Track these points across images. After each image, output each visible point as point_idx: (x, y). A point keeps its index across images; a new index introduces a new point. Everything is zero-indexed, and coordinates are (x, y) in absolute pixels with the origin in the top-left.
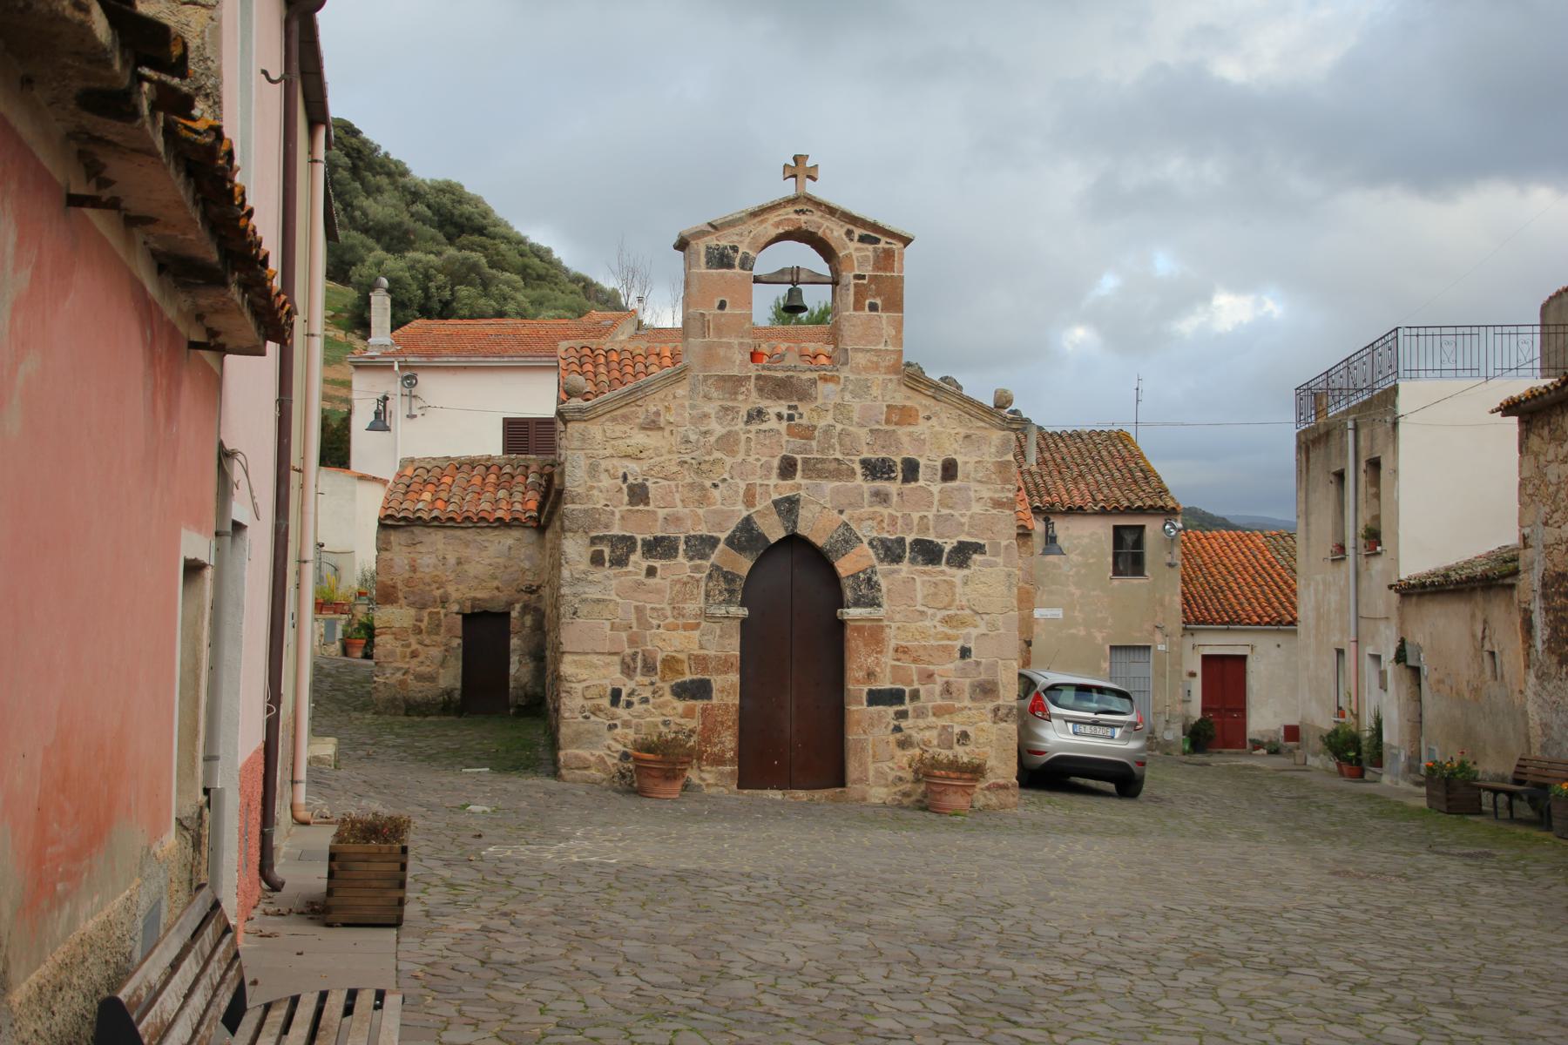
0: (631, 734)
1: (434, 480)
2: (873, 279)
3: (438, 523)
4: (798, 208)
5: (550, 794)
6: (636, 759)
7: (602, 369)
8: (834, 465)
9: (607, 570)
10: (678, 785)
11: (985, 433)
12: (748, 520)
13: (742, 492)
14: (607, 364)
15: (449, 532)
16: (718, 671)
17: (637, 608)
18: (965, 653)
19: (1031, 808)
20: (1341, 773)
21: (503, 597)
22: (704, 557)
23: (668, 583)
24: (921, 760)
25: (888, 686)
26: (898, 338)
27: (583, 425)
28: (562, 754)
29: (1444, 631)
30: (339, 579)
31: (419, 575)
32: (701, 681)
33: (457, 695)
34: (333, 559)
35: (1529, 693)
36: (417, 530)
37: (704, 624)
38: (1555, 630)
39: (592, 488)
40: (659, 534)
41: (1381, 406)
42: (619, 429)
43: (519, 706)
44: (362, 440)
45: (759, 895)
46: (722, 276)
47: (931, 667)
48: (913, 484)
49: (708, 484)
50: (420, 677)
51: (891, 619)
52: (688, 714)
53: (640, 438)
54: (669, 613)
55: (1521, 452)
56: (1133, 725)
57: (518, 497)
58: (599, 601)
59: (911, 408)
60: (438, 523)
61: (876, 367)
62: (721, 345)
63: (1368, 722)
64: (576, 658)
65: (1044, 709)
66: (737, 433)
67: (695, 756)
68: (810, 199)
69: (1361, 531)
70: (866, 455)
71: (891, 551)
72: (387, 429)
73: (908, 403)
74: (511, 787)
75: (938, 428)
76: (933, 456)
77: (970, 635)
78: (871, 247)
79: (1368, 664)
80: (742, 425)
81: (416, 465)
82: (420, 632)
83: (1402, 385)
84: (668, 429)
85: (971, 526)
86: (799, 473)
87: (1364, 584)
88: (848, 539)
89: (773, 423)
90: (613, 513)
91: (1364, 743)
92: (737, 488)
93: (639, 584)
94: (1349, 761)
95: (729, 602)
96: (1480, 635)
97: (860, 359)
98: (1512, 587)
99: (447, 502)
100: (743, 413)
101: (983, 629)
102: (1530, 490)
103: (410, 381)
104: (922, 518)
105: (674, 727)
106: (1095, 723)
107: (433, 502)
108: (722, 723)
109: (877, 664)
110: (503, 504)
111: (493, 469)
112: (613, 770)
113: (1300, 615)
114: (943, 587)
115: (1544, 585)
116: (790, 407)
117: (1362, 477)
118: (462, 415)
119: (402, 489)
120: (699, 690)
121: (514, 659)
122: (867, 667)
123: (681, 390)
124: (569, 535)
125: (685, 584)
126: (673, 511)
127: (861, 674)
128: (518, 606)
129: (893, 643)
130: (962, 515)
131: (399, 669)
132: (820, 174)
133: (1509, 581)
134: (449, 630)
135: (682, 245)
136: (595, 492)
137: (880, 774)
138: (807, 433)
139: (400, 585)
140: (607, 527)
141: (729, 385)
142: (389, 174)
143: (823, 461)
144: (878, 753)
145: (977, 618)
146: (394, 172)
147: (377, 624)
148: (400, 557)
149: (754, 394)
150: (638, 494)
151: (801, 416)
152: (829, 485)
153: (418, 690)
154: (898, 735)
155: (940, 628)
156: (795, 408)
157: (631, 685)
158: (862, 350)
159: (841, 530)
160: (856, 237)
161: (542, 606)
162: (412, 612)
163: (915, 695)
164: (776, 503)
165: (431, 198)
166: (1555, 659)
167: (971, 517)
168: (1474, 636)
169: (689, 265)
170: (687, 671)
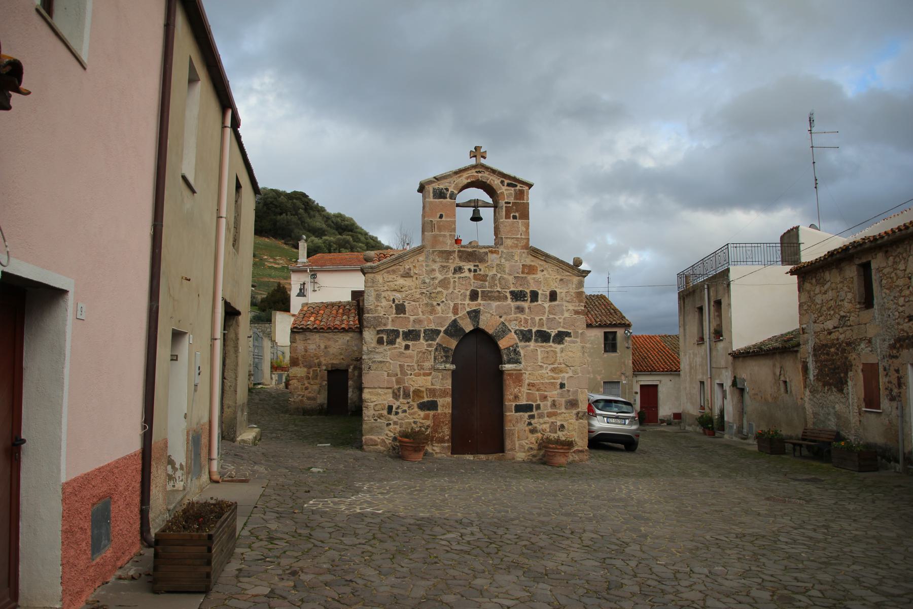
0: (398, 428)
5: (356, 459)
6: (400, 441)
8: (497, 294)
9: (385, 347)
10: (422, 453)
12: (455, 321)
16: (441, 397)
18: (562, 386)
19: (593, 460)
20: (705, 434)
21: (345, 363)
22: (434, 340)
23: (415, 353)
24: (542, 439)
25: (525, 403)
29: (759, 374)
33: (325, 406)
34: (282, 349)
35: (806, 399)
36: (307, 334)
38: (821, 370)
41: (722, 279)
42: (391, 277)
45: (469, 543)
49: (435, 303)
50: (309, 398)
51: (526, 370)
53: (401, 281)
54: (416, 367)
55: (799, 290)
56: (633, 418)
57: (352, 319)
58: (381, 362)
62: (440, 236)
63: (716, 412)
65: (593, 411)
67: (429, 439)
68: (483, 166)
69: (712, 330)
70: (512, 289)
71: (525, 336)
72: (305, 296)
74: (338, 456)
75: (547, 276)
76: (545, 289)
77: (565, 377)
79: (716, 387)
83: (731, 268)
86: (480, 298)
87: (714, 353)
88: (504, 330)
89: (467, 274)
91: (715, 421)
92: (450, 306)
94: (709, 428)
95: (445, 362)
96: (778, 374)
97: (509, 242)
98: (797, 351)
100: (452, 268)
101: (570, 374)
102: (805, 307)
103: (314, 276)
105: (419, 425)
106: (617, 418)
110: (345, 322)
113: (682, 366)
114: (551, 354)
115: (815, 350)
117: (712, 308)
118: (337, 287)
120: (431, 406)
121: (350, 390)
122: (516, 394)
126: (419, 316)
127: (511, 397)
128: (352, 367)
129: (527, 382)
130: (559, 318)
132: (488, 156)
135: (421, 189)
136: (379, 308)
137: (522, 446)
138: (483, 278)
141: (445, 255)
142: (318, 211)
143: (491, 292)
144: (521, 438)
146: (320, 210)
149: (457, 259)
150: (400, 309)
152: (495, 304)
153: (308, 404)
155: (550, 374)
157: (398, 403)
163: (538, 407)
164: (468, 313)
166: (821, 384)
168: (775, 374)
169: (424, 197)
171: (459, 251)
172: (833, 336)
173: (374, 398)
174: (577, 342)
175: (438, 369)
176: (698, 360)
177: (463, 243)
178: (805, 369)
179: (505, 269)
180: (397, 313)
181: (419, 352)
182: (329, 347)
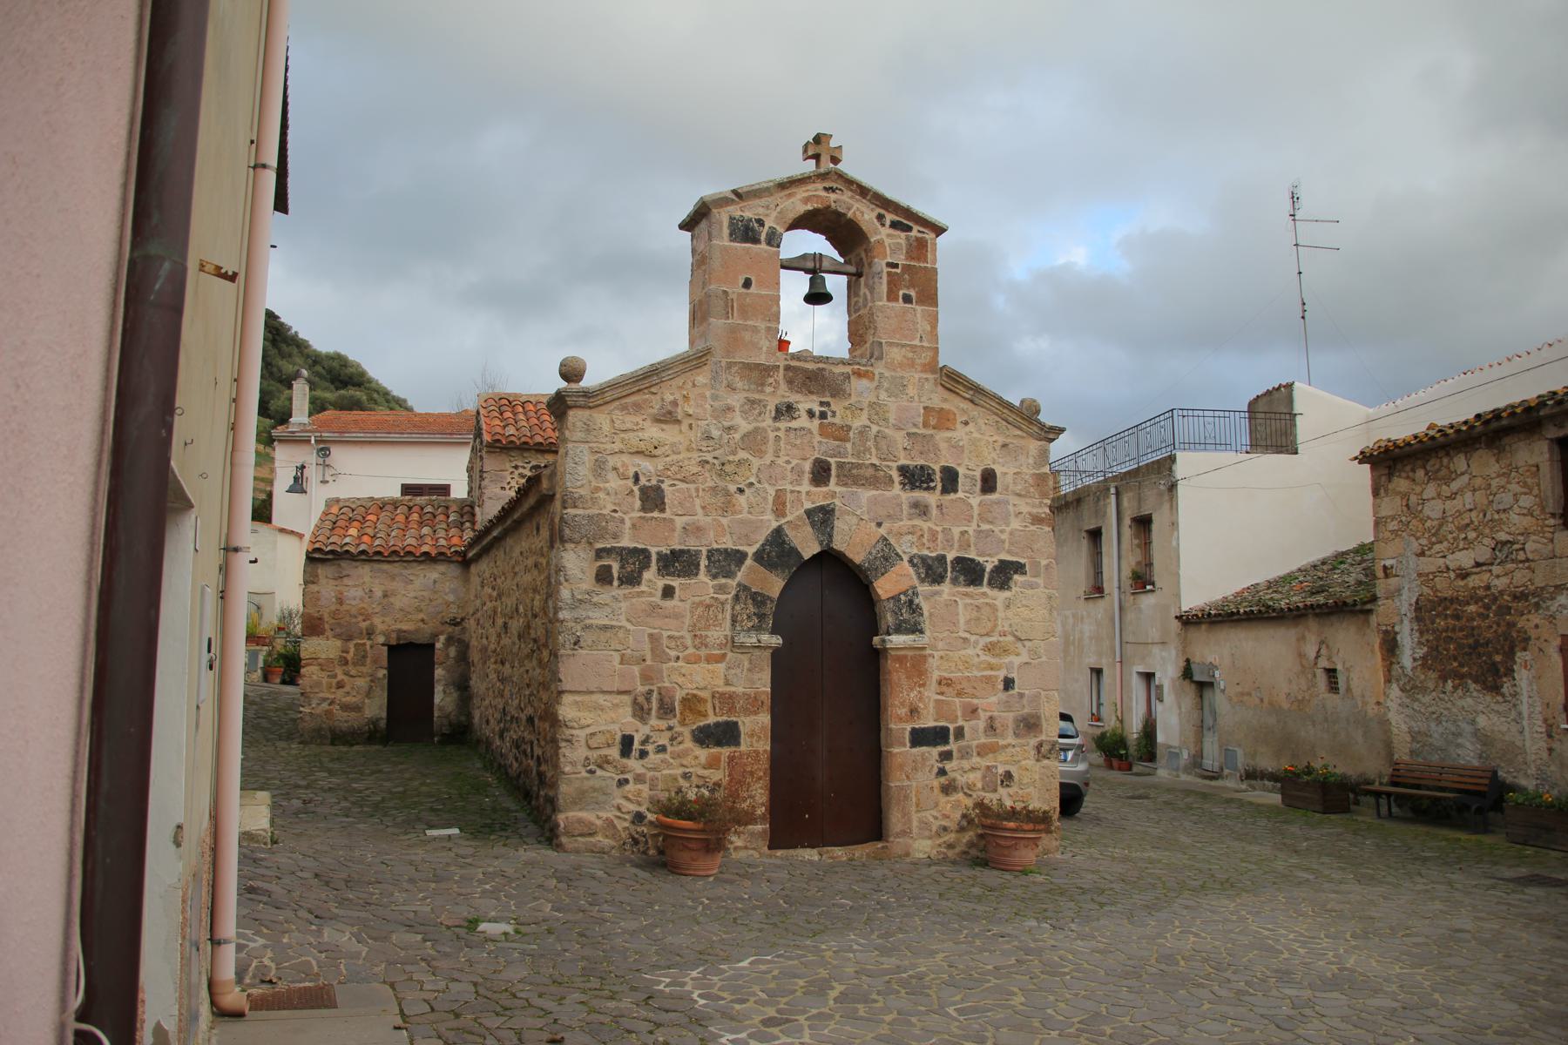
2: (907, 268)
3: (364, 557)
4: (827, 185)
7: (522, 417)
8: (870, 471)
9: (616, 590)
11: (1023, 442)
12: (778, 532)
13: (770, 499)
14: (525, 413)
15: (376, 566)
17: (651, 636)
18: (1008, 684)
20: (1111, 767)
21: (428, 629)
23: (688, 605)
25: (931, 724)
26: (934, 336)
27: (587, 413)
28: (561, 818)
29: (1267, 656)
30: (261, 616)
32: (727, 723)
33: (383, 724)
35: (1393, 705)
36: (344, 564)
37: (730, 655)
39: (598, 489)
40: (677, 547)
41: (1159, 473)
42: (630, 420)
44: (284, 504)
46: (747, 251)
47: (975, 701)
48: (952, 496)
49: (733, 488)
50: (346, 707)
52: (713, 763)
53: (653, 432)
54: (689, 642)
56: (1080, 747)
57: (442, 533)
58: (605, 628)
59: (949, 412)
60: (364, 557)
61: (912, 364)
62: (746, 328)
63: (1135, 727)
64: (578, 698)
66: (764, 430)
69: (1126, 573)
71: (932, 570)
73: (946, 406)
75: (976, 435)
77: (1013, 663)
78: (903, 235)
80: (769, 422)
82: (346, 663)
83: (1179, 455)
84: (686, 422)
85: (1011, 544)
86: (833, 480)
88: (888, 557)
89: (803, 421)
90: (622, 521)
92: (765, 501)
93: (655, 607)
95: (758, 629)
96: (1312, 655)
97: (895, 354)
98: (1370, 611)
99: (374, 537)
100: (771, 407)
101: (1024, 658)
103: (324, 452)
104: (963, 533)
105: (695, 780)
107: (359, 537)
108: (752, 773)
110: (428, 540)
114: (986, 611)
115: (1418, 608)
116: (822, 404)
117: (1127, 532)
119: (328, 525)
120: (725, 734)
121: (438, 689)
122: (909, 703)
123: (702, 378)
124: (569, 546)
125: (708, 607)
126: (694, 520)
127: (903, 711)
128: (442, 638)
129: (936, 675)
131: (324, 700)
133: (1368, 607)
134: (375, 661)
135: (695, 221)
136: (602, 495)
137: (925, 825)
138: (842, 433)
139: (326, 617)
140: (615, 537)
141: (755, 374)
143: (859, 466)
145: (1019, 645)
148: (327, 589)
149: (783, 386)
150: (652, 498)
151: (834, 413)
152: (866, 494)
153: (344, 720)
154: (942, 780)
156: (828, 404)
157: (645, 730)
159: (880, 546)
161: (466, 637)
162: (339, 643)
163: (960, 733)
164: (809, 513)
165: (326, 364)
166: (1433, 675)
167: (1011, 533)
168: (1301, 655)
171: (787, 368)
172: (1473, 581)
173: (587, 717)
174: (1038, 586)
175: (742, 646)
176: (1088, 629)
177: (792, 349)
178: (1390, 645)
179: (889, 411)
180: (643, 509)
181: (696, 605)
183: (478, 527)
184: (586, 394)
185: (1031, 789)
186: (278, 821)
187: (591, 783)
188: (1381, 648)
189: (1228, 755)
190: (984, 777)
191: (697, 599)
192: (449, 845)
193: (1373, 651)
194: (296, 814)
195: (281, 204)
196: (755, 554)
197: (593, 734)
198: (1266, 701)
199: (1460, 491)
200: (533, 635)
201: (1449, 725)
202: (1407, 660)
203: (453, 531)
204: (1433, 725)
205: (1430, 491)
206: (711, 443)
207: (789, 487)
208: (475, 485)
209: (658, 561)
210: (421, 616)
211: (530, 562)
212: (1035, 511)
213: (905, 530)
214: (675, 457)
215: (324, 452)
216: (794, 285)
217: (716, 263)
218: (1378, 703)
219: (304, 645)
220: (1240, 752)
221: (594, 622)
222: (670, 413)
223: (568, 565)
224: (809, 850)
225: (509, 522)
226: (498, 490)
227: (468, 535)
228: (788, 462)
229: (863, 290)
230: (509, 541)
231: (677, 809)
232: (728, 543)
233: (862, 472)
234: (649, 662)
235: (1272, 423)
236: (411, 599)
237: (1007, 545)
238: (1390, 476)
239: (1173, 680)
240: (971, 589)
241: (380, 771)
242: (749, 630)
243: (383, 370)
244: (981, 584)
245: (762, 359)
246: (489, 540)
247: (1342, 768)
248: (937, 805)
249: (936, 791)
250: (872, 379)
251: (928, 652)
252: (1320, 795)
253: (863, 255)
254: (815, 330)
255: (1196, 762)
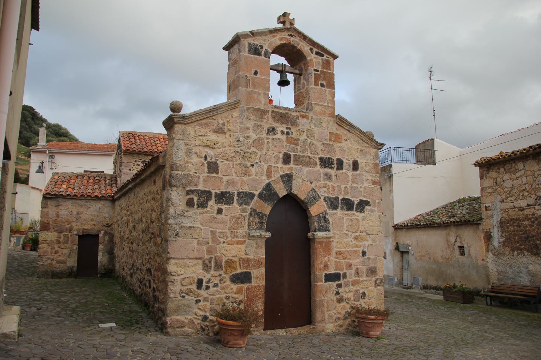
1: (67, 181)
2: (322, 72)
3: (69, 197)
4: (290, 33)
7: (138, 141)
9: (196, 210)
11: (368, 149)
12: (269, 185)
13: (265, 170)
14: (139, 140)
15: (74, 201)
16: (255, 267)
18: (364, 253)
21: (96, 228)
22: (247, 204)
23: (228, 218)
26: (333, 102)
27: (183, 126)
29: (434, 242)
30: (22, 223)
31: (60, 219)
32: (246, 273)
33: (75, 269)
34: (21, 216)
36: (60, 200)
37: (247, 241)
39: (188, 162)
40: (224, 191)
42: (203, 131)
43: (102, 274)
47: (351, 261)
48: (341, 171)
49: (249, 164)
50: (58, 262)
51: (334, 238)
53: (213, 137)
54: (229, 235)
57: (103, 188)
58: (191, 228)
59: (339, 135)
60: (69, 197)
61: (324, 114)
62: (255, 92)
64: (177, 261)
70: (321, 156)
71: (333, 204)
73: (338, 132)
75: (350, 145)
77: (366, 244)
78: (321, 58)
80: (265, 135)
81: (59, 175)
83: (394, 165)
85: (365, 193)
86: (292, 162)
88: (315, 197)
89: (279, 136)
90: (199, 177)
93: (213, 218)
95: (260, 229)
96: (453, 241)
97: (317, 109)
98: (479, 224)
99: (73, 189)
101: (370, 242)
103: (52, 157)
107: (67, 189)
108: (257, 296)
109: (329, 260)
110: (97, 190)
111: (91, 178)
112: (198, 326)
114: (355, 222)
115: (501, 222)
116: (287, 128)
119: (53, 183)
120: (245, 278)
121: (100, 254)
122: (324, 262)
125: (238, 218)
126: (230, 178)
127: (321, 266)
129: (335, 250)
131: (49, 258)
133: (479, 222)
134: (72, 242)
137: (331, 317)
138: (295, 142)
139: (51, 223)
140: (196, 185)
141: (259, 113)
143: (303, 157)
144: (331, 309)
145: (368, 236)
147: (40, 239)
148: (52, 211)
149: (271, 119)
150: (213, 168)
151: (292, 133)
152: (306, 169)
153: (58, 267)
154: (338, 296)
156: (290, 129)
157: (208, 276)
158: (319, 105)
159: (312, 192)
160: (314, 52)
162: (56, 234)
163: (345, 276)
164: (282, 177)
167: (364, 188)
168: (448, 241)
170: (238, 267)
171: (273, 112)
172: (526, 212)
173: (181, 271)
175: (253, 237)
177: (274, 104)
178: (488, 237)
182: (82, 213)
183: (119, 186)
184: (184, 117)
185: (373, 300)
186: (24, 321)
187: (183, 302)
188: (484, 238)
189: (415, 280)
190: (354, 295)
191: (233, 215)
192: (112, 333)
193: (480, 240)
194: (33, 316)
195: (35, 25)
196: (259, 194)
197: (184, 279)
198: (432, 259)
199: (521, 177)
200: (151, 231)
201: (516, 268)
202: (496, 242)
203: (108, 187)
204: (508, 269)
205: (507, 176)
206: (239, 143)
207: (273, 165)
208: (117, 169)
209: (215, 196)
210: (93, 223)
211: (150, 198)
212: (373, 179)
213: (322, 185)
214: (223, 149)
215: (52, 157)
216: (275, 77)
217: (242, 63)
218: (483, 260)
219: (40, 235)
220: (420, 278)
221: (186, 225)
222: (221, 128)
223: (174, 198)
224: (281, 330)
225: (138, 180)
226: (128, 171)
227: (115, 189)
228: (273, 154)
229: (302, 81)
230: (137, 189)
231: (225, 314)
232: (247, 189)
233: (304, 159)
234: (210, 244)
235: (425, 153)
236: (90, 216)
237: (363, 193)
238: (488, 171)
239: (390, 250)
240: (349, 212)
241: (74, 291)
242: (256, 229)
243: (73, 131)
244: (352, 210)
245: (262, 107)
246: (125, 190)
247: (470, 286)
248: (335, 307)
249: (335, 302)
250: (308, 119)
251: (332, 240)
252: (461, 297)
253: (303, 66)
254: (285, 98)
255: (400, 283)
